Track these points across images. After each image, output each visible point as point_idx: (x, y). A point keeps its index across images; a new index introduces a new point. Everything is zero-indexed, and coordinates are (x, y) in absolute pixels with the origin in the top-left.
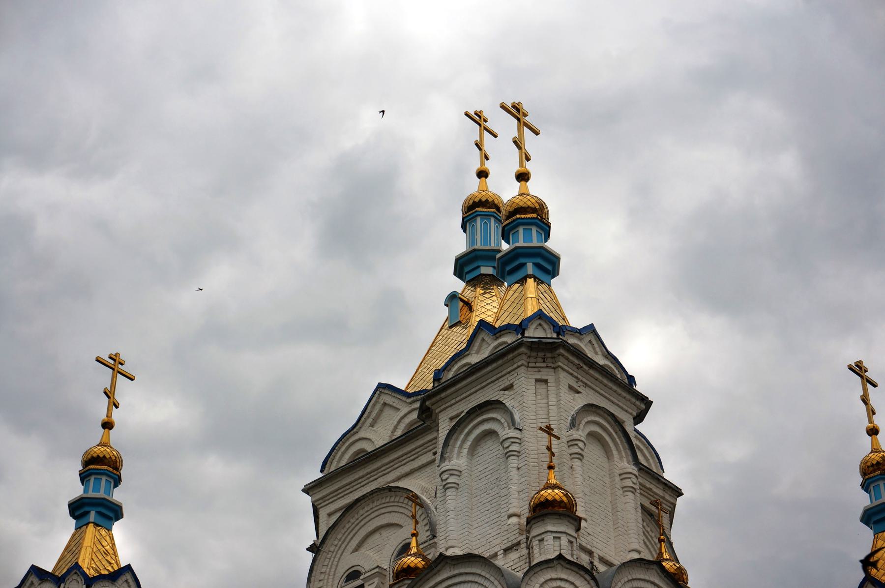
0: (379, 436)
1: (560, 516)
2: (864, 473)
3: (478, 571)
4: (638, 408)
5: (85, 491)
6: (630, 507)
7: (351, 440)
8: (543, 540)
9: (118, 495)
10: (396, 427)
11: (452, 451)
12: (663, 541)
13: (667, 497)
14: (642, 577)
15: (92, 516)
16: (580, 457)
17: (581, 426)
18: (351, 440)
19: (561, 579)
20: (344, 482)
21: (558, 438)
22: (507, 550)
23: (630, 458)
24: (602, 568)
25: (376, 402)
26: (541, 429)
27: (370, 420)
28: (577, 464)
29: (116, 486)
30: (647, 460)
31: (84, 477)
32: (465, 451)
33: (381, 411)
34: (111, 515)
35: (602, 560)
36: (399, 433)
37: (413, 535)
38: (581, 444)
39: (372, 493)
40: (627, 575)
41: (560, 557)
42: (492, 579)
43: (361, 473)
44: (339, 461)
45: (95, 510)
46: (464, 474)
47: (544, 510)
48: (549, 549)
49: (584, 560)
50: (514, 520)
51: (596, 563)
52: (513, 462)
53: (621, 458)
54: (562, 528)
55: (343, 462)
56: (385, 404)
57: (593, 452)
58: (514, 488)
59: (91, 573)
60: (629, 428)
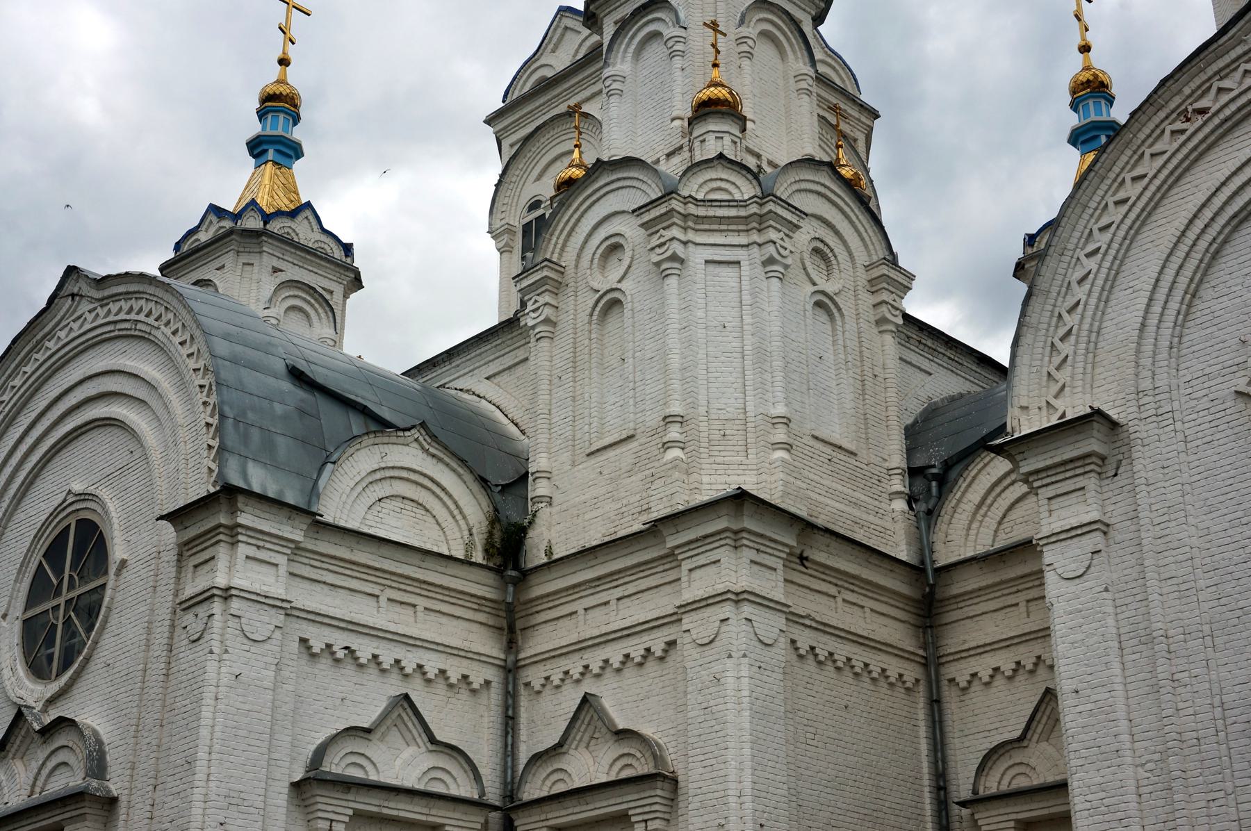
0: (560, 60)
1: (723, 114)
2: (1073, 92)
3: (636, 175)
4: (817, 7)
5: (263, 129)
6: (806, 112)
7: (533, 68)
8: (704, 141)
9: (297, 134)
10: (577, 51)
11: (616, 57)
12: (841, 146)
13: (863, 119)
14: (811, 178)
15: (271, 154)
16: (749, 55)
17: (752, 24)
18: (533, 68)
19: (721, 180)
20: (525, 111)
21: (725, 35)
22: (669, 155)
23: (807, 60)
24: (769, 170)
25: (558, 26)
26: (705, 24)
27: (551, 46)
28: (746, 63)
29: (295, 124)
30: (843, 81)
31: (262, 114)
32: (629, 55)
33: (563, 35)
34: (291, 153)
35: (770, 163)
36: (580, 56)
37: (576, 146)
38: (750, 42)
39: (553, 119)
40: (794, 176)
41: (721, 156)
42: (649, 182)
43: (542, 100)
44: (522, 87)
45: (274, 148)
46: (628, 80)
47: (706, 109)
48: (711, 148)
49: (751, 162)
50: (677, 123)
51: (765, 166)
52: (678, 63)
53: (797, 58)
54: (725, 128)
55: (526, 89)
56: (566, 28)
57: (765, 51)
58: (678, 90)
59: (269, 210)
60: (807, 27)
